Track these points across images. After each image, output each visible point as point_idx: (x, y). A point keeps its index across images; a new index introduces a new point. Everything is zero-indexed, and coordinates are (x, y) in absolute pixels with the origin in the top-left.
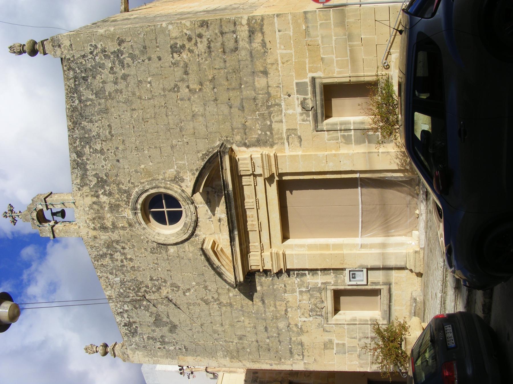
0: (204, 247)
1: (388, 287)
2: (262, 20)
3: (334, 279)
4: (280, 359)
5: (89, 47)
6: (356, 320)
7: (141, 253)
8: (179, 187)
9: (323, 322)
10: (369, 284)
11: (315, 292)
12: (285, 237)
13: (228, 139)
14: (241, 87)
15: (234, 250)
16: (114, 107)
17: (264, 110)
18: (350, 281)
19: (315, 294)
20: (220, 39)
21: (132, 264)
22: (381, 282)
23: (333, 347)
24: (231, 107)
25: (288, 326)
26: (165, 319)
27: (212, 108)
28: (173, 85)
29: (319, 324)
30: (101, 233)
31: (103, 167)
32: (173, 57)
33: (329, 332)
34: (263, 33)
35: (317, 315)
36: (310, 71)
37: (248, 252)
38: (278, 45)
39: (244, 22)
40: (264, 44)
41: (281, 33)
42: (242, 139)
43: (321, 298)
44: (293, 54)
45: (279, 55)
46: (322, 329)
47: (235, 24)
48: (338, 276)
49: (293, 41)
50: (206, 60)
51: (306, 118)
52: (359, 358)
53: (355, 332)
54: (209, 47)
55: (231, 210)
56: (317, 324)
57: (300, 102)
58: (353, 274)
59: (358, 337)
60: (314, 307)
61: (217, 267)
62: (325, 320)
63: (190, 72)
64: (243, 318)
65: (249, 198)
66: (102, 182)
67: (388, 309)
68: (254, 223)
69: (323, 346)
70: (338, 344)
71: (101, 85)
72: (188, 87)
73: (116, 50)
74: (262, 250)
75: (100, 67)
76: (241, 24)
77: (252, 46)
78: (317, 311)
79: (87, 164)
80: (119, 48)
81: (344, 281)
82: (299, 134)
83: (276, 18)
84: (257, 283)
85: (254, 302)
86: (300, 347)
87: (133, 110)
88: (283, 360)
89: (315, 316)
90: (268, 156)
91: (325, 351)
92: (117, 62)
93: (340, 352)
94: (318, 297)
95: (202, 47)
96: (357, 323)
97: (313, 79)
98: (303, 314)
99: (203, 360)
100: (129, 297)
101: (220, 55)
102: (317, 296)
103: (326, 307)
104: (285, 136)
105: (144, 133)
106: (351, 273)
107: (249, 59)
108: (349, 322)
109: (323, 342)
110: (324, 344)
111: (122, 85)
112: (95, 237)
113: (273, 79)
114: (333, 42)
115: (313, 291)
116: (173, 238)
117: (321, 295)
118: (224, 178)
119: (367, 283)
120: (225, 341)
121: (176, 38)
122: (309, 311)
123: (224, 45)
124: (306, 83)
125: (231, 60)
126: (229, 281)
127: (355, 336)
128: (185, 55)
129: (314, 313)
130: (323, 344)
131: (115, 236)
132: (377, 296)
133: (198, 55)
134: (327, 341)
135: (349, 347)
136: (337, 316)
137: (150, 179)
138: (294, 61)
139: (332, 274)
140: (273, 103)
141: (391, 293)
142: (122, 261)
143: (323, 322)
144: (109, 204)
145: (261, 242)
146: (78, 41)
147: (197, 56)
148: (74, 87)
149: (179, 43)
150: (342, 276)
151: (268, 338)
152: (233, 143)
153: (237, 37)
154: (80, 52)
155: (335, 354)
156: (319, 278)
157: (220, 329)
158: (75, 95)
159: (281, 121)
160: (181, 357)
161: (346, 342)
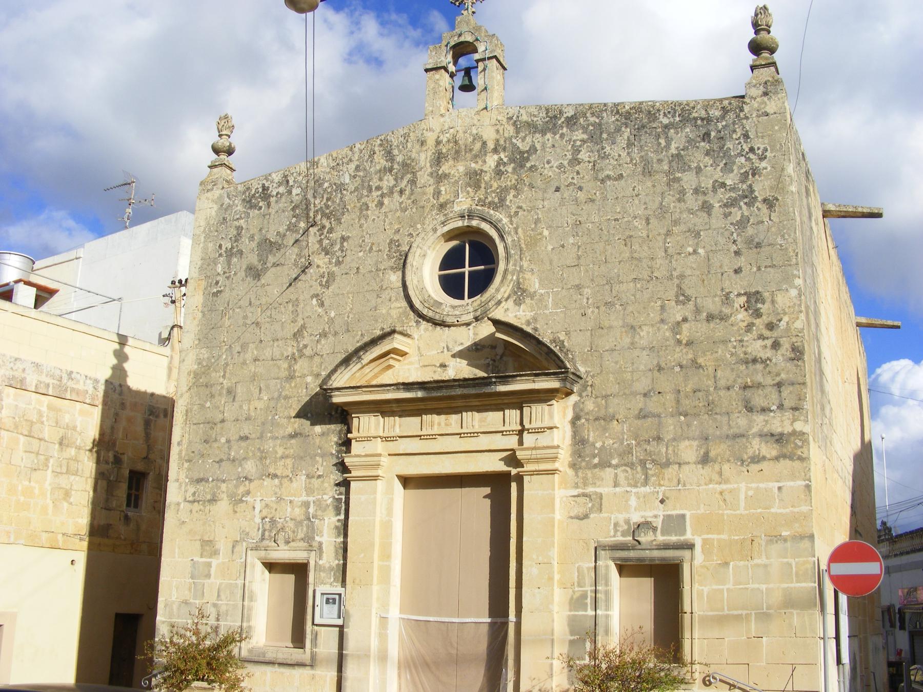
0: (396, 336)
1: (308, 662)
2: (801, 459)
3: (327, 565)
4: (189, 461)
5: (762, 147)
6: (252, 601)
7: (391, 223)
8: (506, 295)
9: (251, 541)
10: (316, 628)
11: (305, 529)
12: (407, 481)
13: (589, 388)
14: (681, 414)
15: (388, 388)
16: (654, 186)
17: (638, 454)
18: (322, 594)
19: (302, 530)
20: (769, 381)
21: (372, 205)
22: (316, 650)
23: (206, 557)
24: (645, 395)
25: (246, 478)
26: (271, 259)
27: (645, 360)
28: (688, 292)
29: (248, 534)
30: (430, 153)
31: (548, 162)
32: (739, 295)
33: (233, 552)
34: (777, 458)
35: (264, 531)
36: (705, 542)
37: (384, 414)
38: (754, 485)
39: (799, 426)
40: (757, 459)
41: (776, 491)
42: (587, 414)
43: (293, 541)
44: (738, 512)
45: (736, 486)
46: (239, 539)
47: (795, 409)
48: (332, 574)
49: (760, 513)
50: (732, 355)
51: (621, 529)
52: (183, 602)
53: (228, 599)
54: (755, 361)
55: (460, 386)
56: (247, 530)
57: (649, 520)
58: (334, 600)
59: (220, 602)
60: (279, 526)
61: (360, 358)
62: (254, 545)
63: (712, 325)
64: (266, 398)
65: (481, 421)
66: (520, 159)
67: (267, 659)
68: (436, 427)
69: (208, 539)
70: (209, 565)
71: (694, 165)
72: (685, 320)
73: (756, 194)
74: (386, 439)
75: (725, 164)
76: (794, 421)
77: (754, 437)
78: (270, 531)
79: (555, 134)
80: (760, 199)
81: (322, 583)
82: (592, 516)
83: (804, 483)
84: (328, 426)
85: (293, 420)
86: (209, 497)
87: (647, 220)
88: (186, 465)
89: (263, 526)
90: (554, 459)
91: (198, 543)
92: (734, 195)
93: (195, 568)
94: (296, 534)
95: (757, 348)
96: (246, 603)
97: (690, 547)
98: (267, 506)
99: (196, 322)
100: (315, 197)
101: (740, 381)
102: (298, 532)
103: (278, 548)
104: (590, 490)
105: (605, 238)
106: (337, 597)
107: (731, 432)
108: (248, 587)
109: (214, 538)
110: (211, 541)
111: (692, 202)
112: (423, 143)
113: (692, 473)
114: (756, 586)
115: (308, 527)
116: (415, 282)
117: (300, 540)
118: (518, 378)
119: (317, 625)
120: (227, 364)
121: (773, 302)
122: (273, 517)
123: (758, 387)
124: (683, 532)
125: (731, 400)
126: (333, 378)
127: (223, 596)
128: (742, 317)
129: (267, 527)
130: (211, 538)
131: (424, 178)
132: (293, 642)
133: (741, 341)
134: (217, 547)
135: (204, 585)
136: (260, 567)
137: (523, 246)
138: (725, 512)
139: (337, 562)
140: (650, 472)
141: (296, 667)
142: (378, 188)
143: (251, 541)
144: (482, 171)
145: (399, 437)
146: (773, 127)
147: (739, 338)
148: (691, 117)
149: (764, 308)
150: (332, 580)
151: (228, 441)
152: (580, 395)
153: (771, 411)
154: (753, 130)
155: (192, 560)
156: (329, 539)
157: (249, 356)
158: (677, 119)
159: (616, 485)
160: (204, 283)
161: (212, 579)
